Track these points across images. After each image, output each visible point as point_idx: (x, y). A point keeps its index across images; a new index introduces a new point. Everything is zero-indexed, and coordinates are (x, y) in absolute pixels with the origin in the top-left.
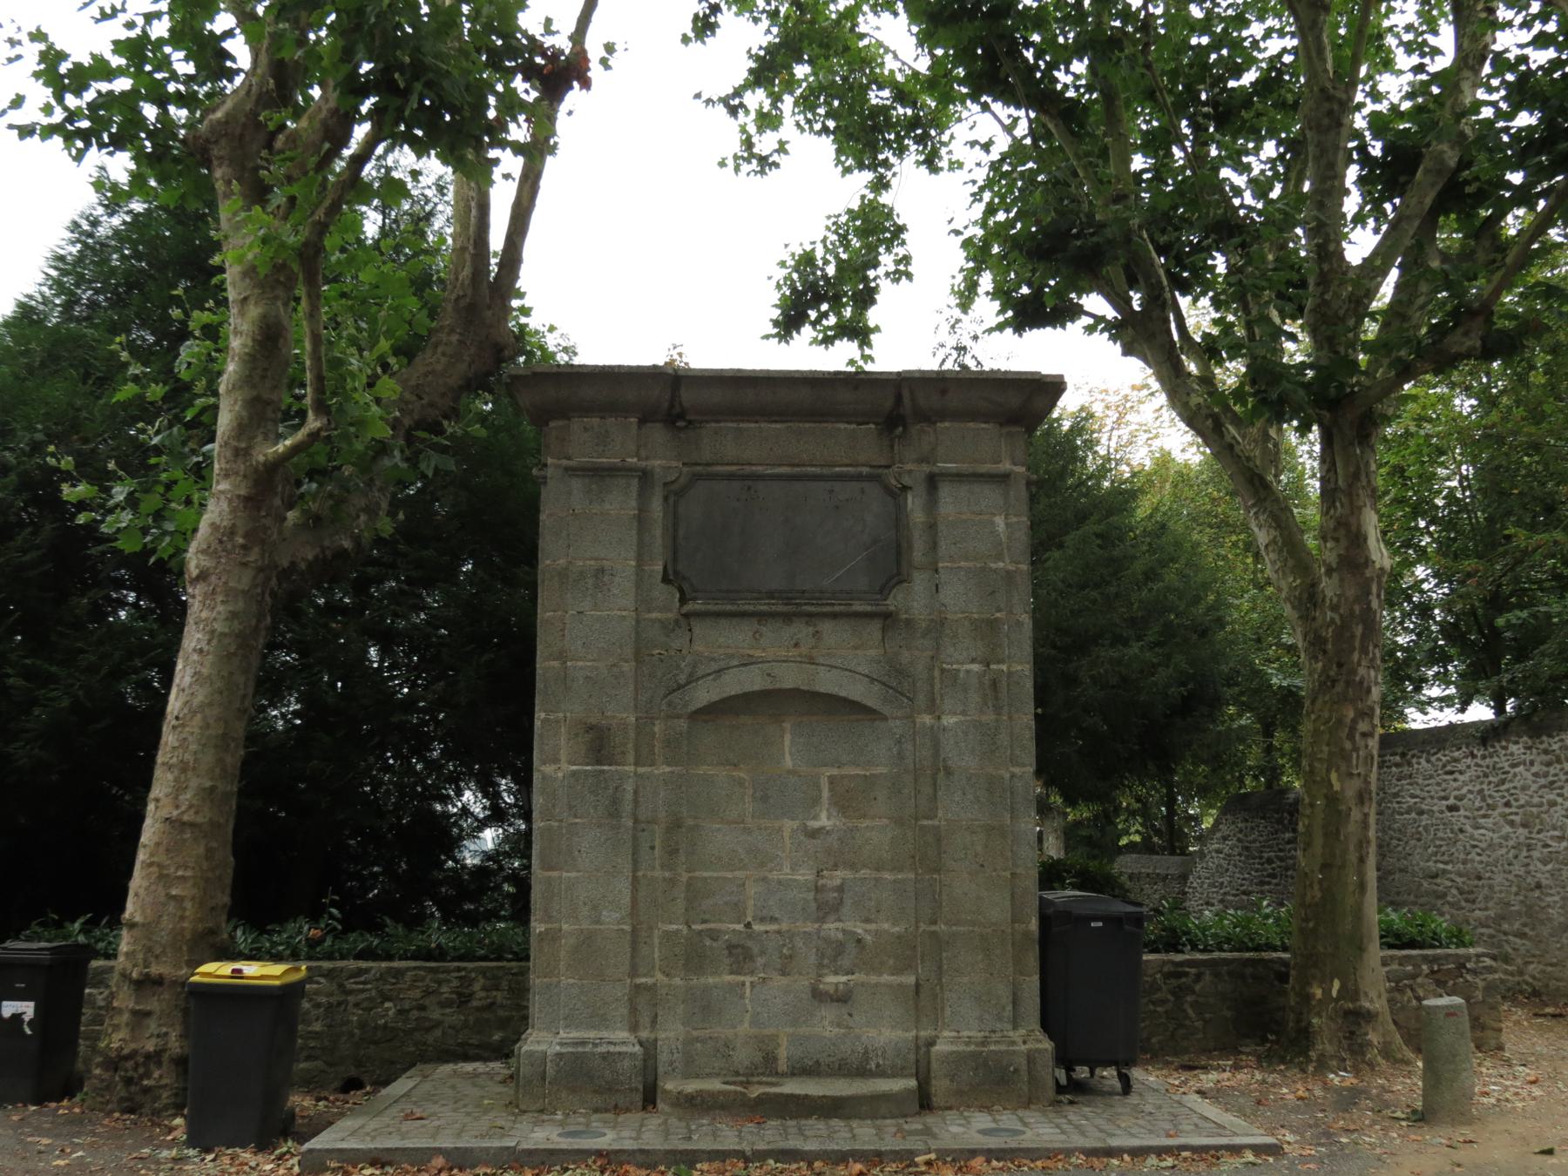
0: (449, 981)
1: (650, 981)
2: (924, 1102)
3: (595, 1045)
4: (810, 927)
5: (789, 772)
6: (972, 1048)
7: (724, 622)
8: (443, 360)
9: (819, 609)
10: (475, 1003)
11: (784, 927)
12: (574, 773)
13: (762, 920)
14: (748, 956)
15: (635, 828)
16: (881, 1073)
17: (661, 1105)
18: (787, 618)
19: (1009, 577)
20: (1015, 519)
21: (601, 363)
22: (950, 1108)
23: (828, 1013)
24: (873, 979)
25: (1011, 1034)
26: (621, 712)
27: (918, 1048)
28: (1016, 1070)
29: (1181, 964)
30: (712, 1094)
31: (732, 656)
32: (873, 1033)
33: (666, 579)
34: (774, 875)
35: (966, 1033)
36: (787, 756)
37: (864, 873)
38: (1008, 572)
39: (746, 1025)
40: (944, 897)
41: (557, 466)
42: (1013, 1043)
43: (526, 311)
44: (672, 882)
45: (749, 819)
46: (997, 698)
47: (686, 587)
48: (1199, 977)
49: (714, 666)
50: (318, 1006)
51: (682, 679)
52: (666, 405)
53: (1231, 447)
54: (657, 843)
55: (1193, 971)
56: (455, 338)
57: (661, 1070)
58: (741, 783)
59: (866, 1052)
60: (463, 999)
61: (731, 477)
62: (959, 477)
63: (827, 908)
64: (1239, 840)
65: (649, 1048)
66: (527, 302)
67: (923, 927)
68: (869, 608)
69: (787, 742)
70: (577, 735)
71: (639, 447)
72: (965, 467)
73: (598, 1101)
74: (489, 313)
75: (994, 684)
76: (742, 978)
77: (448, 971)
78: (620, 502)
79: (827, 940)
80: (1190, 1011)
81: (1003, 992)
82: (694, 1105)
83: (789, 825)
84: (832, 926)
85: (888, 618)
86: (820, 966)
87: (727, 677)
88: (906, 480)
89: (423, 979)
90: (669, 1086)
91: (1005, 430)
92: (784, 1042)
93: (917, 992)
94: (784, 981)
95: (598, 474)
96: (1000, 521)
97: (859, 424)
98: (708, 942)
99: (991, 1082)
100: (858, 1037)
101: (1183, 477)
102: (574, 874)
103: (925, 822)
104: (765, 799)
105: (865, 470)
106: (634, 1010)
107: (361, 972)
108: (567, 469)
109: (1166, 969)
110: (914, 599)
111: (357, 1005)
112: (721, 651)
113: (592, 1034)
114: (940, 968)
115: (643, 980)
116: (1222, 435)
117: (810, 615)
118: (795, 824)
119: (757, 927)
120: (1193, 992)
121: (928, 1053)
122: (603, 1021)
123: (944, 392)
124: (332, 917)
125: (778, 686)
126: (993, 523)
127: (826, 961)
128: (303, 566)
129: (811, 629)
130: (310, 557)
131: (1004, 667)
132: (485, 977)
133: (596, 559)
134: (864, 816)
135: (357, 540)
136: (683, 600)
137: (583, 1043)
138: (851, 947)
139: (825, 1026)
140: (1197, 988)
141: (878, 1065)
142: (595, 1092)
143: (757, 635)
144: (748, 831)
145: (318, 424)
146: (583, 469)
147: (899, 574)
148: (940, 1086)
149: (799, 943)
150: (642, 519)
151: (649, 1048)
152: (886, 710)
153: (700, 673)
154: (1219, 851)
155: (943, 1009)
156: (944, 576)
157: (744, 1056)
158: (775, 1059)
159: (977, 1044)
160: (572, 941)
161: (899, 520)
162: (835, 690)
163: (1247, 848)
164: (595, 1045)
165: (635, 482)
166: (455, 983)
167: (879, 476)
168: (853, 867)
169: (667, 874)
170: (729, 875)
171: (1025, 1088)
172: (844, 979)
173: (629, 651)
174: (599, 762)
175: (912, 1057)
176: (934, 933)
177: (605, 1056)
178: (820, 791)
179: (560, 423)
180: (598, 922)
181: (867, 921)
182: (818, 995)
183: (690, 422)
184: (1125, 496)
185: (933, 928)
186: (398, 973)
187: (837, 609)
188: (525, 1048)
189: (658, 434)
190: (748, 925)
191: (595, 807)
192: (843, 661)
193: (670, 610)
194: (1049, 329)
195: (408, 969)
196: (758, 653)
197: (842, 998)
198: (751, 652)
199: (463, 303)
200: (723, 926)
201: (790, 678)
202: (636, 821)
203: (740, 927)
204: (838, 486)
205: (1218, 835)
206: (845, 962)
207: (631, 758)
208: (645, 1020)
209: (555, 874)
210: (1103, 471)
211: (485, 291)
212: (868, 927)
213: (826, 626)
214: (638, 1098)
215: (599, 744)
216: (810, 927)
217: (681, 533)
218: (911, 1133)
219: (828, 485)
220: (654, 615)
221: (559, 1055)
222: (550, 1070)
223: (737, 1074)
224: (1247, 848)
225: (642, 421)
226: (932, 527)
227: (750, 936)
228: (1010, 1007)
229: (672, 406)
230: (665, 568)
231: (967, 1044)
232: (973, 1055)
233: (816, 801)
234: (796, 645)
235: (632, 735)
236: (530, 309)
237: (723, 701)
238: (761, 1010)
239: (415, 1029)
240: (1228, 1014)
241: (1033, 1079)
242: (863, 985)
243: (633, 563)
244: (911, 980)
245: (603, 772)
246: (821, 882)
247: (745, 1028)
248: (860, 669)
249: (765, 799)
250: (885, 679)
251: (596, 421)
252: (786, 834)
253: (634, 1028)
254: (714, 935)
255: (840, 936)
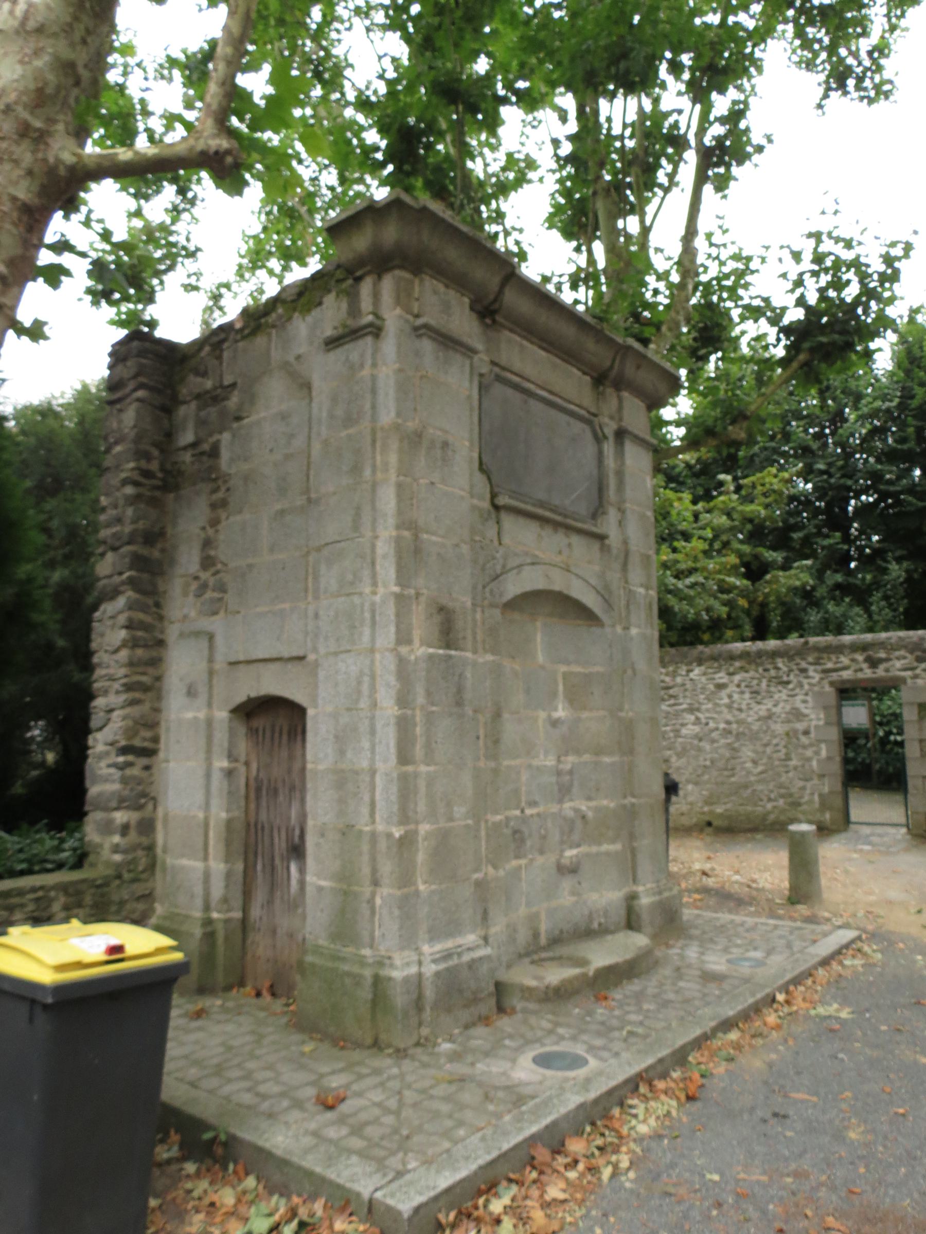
0: (22, 906)
4: (554, 808)
7: (522, 521)
18: (556, 525)
23: (567, 883)
24: (594, 849)
32: (594, 896)
37: (586, 757)
51: (499, 569)
52: (492, 297)
54: (482, 733)
59: (591, 914)
61: (516, 387)
63: (564, 792)
69: (539, 638)
73: (465, 1015)
77: (21, 893)
83: (542, 715)
86: (562, 842)
92: (543, 916)
105: (583, 412)
119: (528, 812)
138: (579, 824)
153: (509, 566)
166: (31, 907)
174: (448, 646)
181: (589, 799)
190: (523, 811)
194: (36, 402)
197: (573, 870)
206: (576, 837)
213: (575, 539)
216: (554, 808)
222: (429, 993)
226: (620, 474)
229: (495, 300)
245: (450, 657)
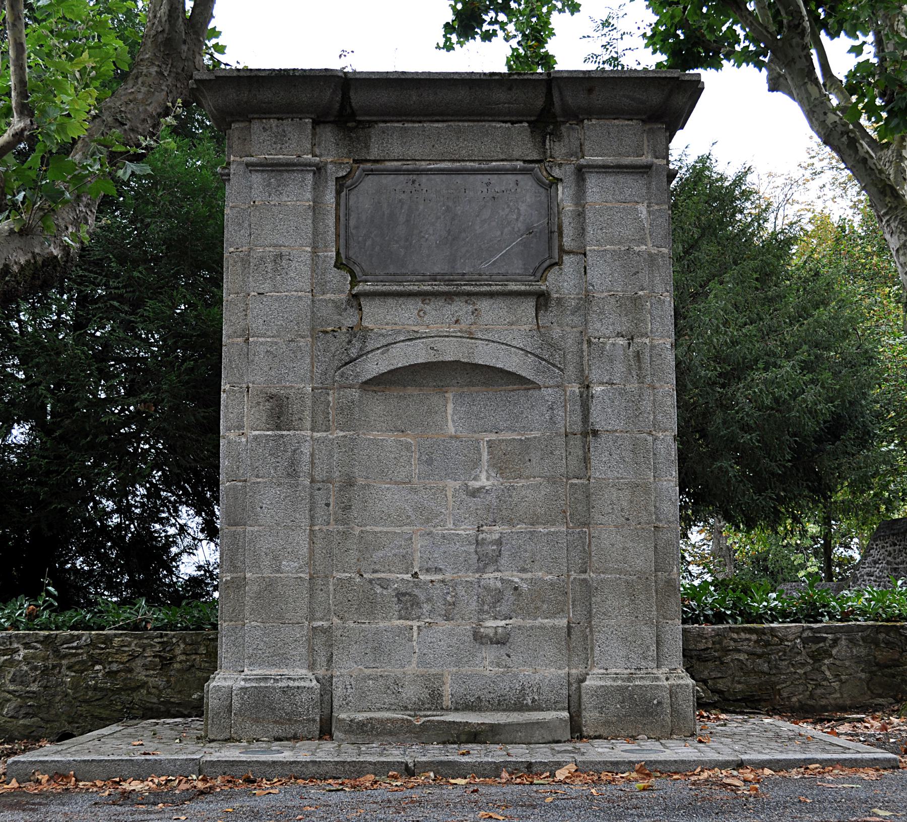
0: (152, 646)
1: (326, 624)
2: (577, 731)
3: (276, 681)
4: (472, 577)
5: (451, 437)
6: (619, 683)
7: (391, 301)
8: (143, 89)
9: (477, 289)
10: (177, 666)
11: (448, 576)
12: (256, 438)
13: (428, 570)
14: (415, 603)
15: (311, 487)
16: (536, 707)
17: (337, 734)
18: (449, 296)
19: (652, 259)
20: (656, 207)
21: (277, 67)
22: (599, 737)
23: (489, 654)
24: (529, 623)
25: (655, 671)
26: (299, 382)
27: (570, 684)
28: (659, 703)
29: (819, 630)
30: (381, 721)
31: (399, 332)
32: (528, 671)
33: (338, 265)
34: (438, 531)
35: (614, 670)
36: (450, 423)
37: (521, 527)
38: (650, 255)
39: (414, 665)
40: (593, 548)
41: (240, 163)
42: (657, 679)
43: (221, 49)
44: (345, 535)
45: (415, 480)
46: (640, 368)
47: (357, 270)
48: (835, 641)
49: (384, 342)
50: (35, 668)
52: (337, 106)
53: (864, 161)
55: (830, 636)
56: (154, 70)
57: (336, 703)
58: (408, 447)
60: (165, 663)
61: (397, 172)
62: (604, 169)
63: (487, 560)
64: (888, 563)
65: (326, 685)
66: (221, 41)
67: (574, 575)
68: (523, 288)
69: (450, 407)
70: (258, 403)
71: (313, 145)
72: (610, 160)
74: (185, 48)
75: (638, 355)
76: (409, 623)
78: (298, 194)
79: (487, 588)
80: (827, 673)
81: (648, 634)
82: (363, 731)
84: (491, 575)
85: (542, 300)
86: (481, 611)
87: (395, 350)
88: (557, 172)
89: (129, 645)
90: (343, 716)
91: (647, 127)
92: (448, 679)
93: (569, 634)
94: (448, 625)
95: (275, 168)
96: (642, 209)
97: (513, 123)
98: (379, 590)
99: (639, 713)
100: (516, 676)
101: (842, 233)
102: (256, 528)
103: (575, 481)
104: (430, 462)
105: (519, 164)
106: (312, 650)
107: (73, 638)
108: (248, 165)
109: (805, 635)
110: (563, 282)
111: (69, 668)
112: (389, 327)
113: (273, 672)
114: (590, 612)
115: (320, 623)
116: (857, 151)
117: (469, 294)
118: (457, 484)
120: (831, 656)
121: (579, 688)
122: (283, 660)
123: (590, 91)
124: (49, 594)
125: (441, 359)
126: (636, 209)
127: (486, 607)
128: (15, 268)
129: (471, 308)
130: (22, 262)
131: (647, 341)
132: (185, 642)
133: (275, 246)
134: (520, 477)
135: (66, 248)
136: (354, 283)
137: (266, 679)
138: (509, 594)
139: (486, 665)
140: (834, 652)
141: (534, 700)
142: (275, 722)
143: (421, 313)
144: (414, 491)
145: (22, 125)
146: (261, 165)
147: (551, 257)
148: (590, 717)
149: (461, 591)
150: (316, 208)
151: (326, 685)
152: (539, 380)
154: (870, 574)
155: (592, 649)
156: (590, 260)
157: (411, 693)
158: (441, 696)
159: (623, 680)
160: (255, 588)
161: (552, 209)
162: (492, 363)
163: (895, 570)
164: (276, 681)
165: (310, 177)
167: (532, 169)
168: (510, 522)
169: (341, 528)
170: (398, 530)
171: (668, 719)
172: (503, 623)
173: (305, 328)
174: (278, 428)
175: (565, 692)
176: (585, 580)
177: (285, 690)
178: (480, 454)
179: (242, 125)
180: (278, 571)
181: (524, 570)
182: (478, 638)
183: (360, 122)
184: (781, 244)
185: (583, 576)
186: (108, 640)
187: (494, 288)
188: (214, 684)
189: (328, 134)
190: (415, 575)
191: (275, 468)
192: (500, 336)
193: (343, 292)
195: (115, 635)
196: (422, 329)
197: (501, 641)
198: (416, 329)
199: (161, 38)
200: (392, 576)
201: (451, 351)
202: (313, 481)
203: (408, 577)
204: (494, 179)
205: (870, 559)
206: (504, 608)
207: (308, 424)
208: (322, 660)
209: (239, 529)
210: (760, 218)
211: (181, 26)
212: (524, 576)
213: (484, 305)
214: (315, 728)
215: (279, 413)
216: (472, 577)
217: (352, 223)
218: (559, 752)
219: (486, 178)
220: (328, 296)
221: (244, 689)
222: (236, 704)
223: (406, 708)
224: (895, 570)
225: (316, 123)
226: (580, 215)
227: (416, 585)
228: (654, 647)
229: (342, 107)
230: (338, 254)
231: (614, 680)
232: (620, 689)
233: (476, 463)
234: (457, 322)
235: (309, 403)
236: (224, 47)
237: (390, 372)
238: (428, 655)
239: (121, 689)
240: (863, 676)
241: (675, 712)
242: (519, 628)
243: (309, 249)
244: (564, 622)
246: (481, 536)
247: (412, 668)
248: (514, 343)
249: (430, 462)
250: (538, 352)
251: (274, 123)
252: (450, 494)
253: (312, 667)
254: (384, 584)
255: (499, 584)
